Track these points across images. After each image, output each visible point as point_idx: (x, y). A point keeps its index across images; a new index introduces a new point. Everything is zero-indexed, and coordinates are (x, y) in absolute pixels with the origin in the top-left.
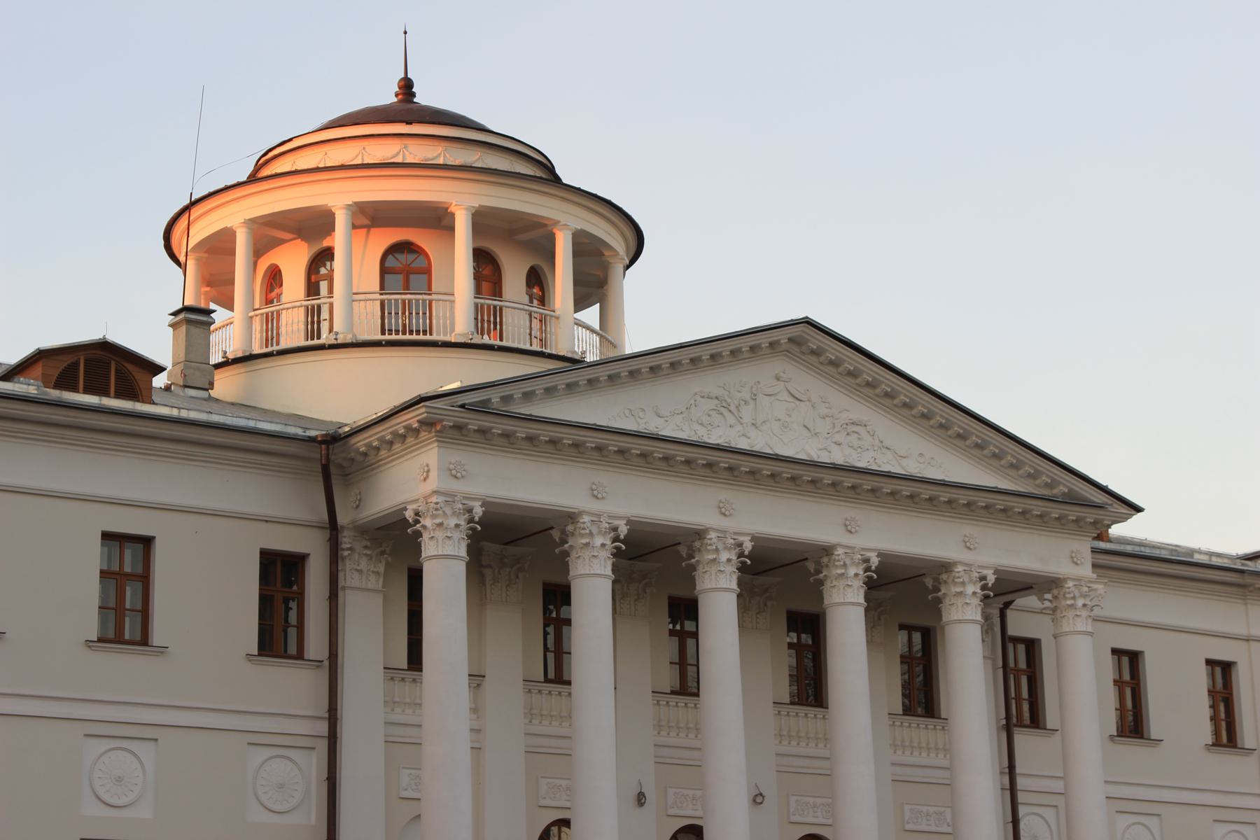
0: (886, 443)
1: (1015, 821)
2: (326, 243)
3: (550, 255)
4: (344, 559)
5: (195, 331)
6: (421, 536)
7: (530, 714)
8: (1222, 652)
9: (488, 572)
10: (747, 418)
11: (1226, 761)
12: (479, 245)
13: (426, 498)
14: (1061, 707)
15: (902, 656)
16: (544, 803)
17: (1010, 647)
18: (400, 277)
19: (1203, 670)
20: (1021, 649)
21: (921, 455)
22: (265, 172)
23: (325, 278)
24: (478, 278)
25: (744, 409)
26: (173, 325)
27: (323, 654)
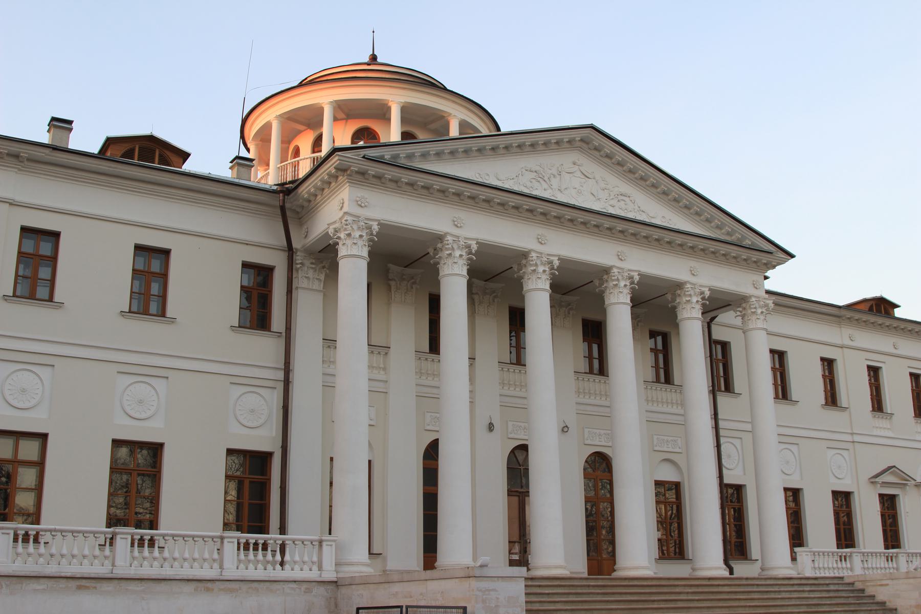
0: (642, 208)
1: (718, 446)
4: (297, 270)
5: (243, 170)
6: (338, 244)
7: (420, 373)
8: (829, 354)
9: (393, 283)
10: (555, 186)
11: (832, 414)
12: (407, 129)
13: (341, 219)
15: (651, 349)
16: (428, 428)
17: (713, 346)
19: (819, 362)
20: (719, 347)
21: (663, 217)
25: (553, 179)
26: (230, 168)
27: (282, 329)
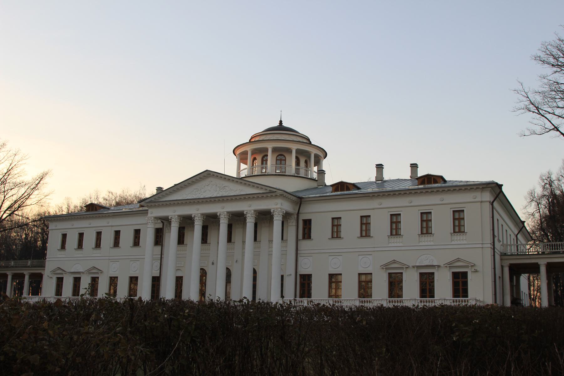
2: (266, 154)
3: (309, 157)
14: (495, 294)
22: (253, 140)
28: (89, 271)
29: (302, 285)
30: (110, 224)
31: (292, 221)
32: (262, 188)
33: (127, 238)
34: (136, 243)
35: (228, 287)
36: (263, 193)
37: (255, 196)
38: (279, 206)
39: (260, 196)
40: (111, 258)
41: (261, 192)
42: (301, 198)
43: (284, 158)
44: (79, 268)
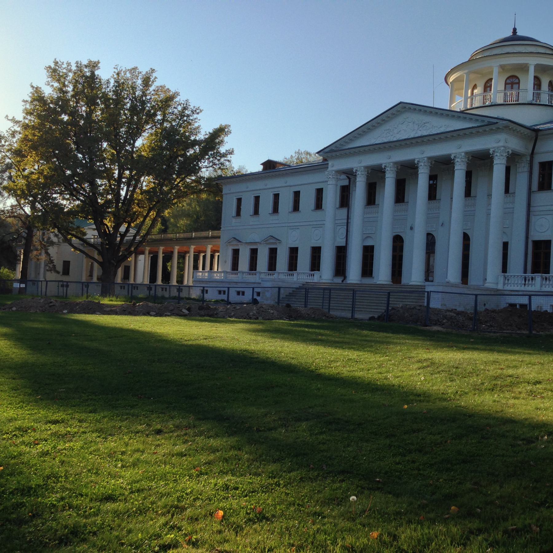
18: (510, 85)
23: (489, 87)
24: (534, 85)
28: (266, 241)
29: (536, 256)
30: (288, 184)
31: (523, 165)
32: (477, 120)
33: (308, 200)
34: (319, 205)
35: (431, 259)
36: (478, 127)
37: (467, 132)
38: (501, 144)
39: (474, 131)
40: (291, 225)
41: (476, 125)
42: (537, 131)
43: (517, 81)
44: (255, 237)
